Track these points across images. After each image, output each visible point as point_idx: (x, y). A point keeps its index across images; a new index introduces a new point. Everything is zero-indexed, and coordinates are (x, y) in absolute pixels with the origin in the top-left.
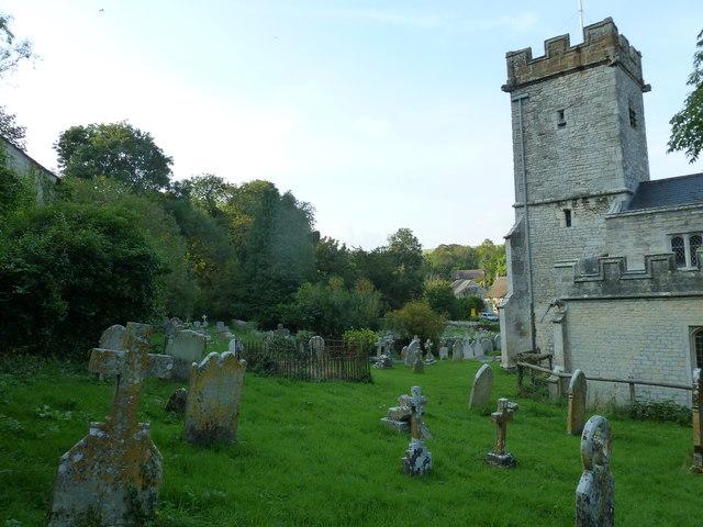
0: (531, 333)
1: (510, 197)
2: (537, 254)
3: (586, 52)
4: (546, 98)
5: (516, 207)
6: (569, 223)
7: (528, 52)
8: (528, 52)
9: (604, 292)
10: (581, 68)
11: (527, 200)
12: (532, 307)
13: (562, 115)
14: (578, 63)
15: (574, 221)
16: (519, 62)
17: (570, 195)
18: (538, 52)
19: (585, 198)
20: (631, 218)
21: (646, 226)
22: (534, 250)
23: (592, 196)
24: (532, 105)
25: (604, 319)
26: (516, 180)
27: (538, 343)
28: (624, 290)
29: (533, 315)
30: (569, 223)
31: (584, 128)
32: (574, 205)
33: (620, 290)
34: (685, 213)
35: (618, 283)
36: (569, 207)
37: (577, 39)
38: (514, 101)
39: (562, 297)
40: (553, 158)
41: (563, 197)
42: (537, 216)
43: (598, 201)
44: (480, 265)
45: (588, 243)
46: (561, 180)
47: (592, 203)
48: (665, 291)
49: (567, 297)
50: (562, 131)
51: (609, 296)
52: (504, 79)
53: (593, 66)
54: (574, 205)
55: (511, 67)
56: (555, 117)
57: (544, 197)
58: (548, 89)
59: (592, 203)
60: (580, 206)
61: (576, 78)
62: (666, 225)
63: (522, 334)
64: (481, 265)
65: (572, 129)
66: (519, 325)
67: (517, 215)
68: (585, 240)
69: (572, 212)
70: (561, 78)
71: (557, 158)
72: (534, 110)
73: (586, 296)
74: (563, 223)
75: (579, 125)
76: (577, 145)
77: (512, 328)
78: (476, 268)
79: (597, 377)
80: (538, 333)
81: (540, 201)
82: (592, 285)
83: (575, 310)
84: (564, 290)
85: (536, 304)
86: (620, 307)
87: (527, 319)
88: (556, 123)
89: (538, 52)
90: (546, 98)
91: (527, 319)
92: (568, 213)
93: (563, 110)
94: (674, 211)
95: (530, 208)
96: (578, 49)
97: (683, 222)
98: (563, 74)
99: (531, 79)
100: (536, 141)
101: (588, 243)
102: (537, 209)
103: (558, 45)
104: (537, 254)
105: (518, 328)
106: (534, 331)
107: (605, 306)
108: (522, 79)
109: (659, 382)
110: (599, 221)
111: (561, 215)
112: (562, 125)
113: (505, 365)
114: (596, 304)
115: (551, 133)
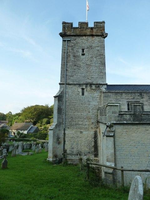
0: (63, 142)
1: (58, 79)
2: (69, 106)
3: (95, 30)
4: (77, 43)
5: (60, 84)
6: (83, 94)
7: (72, 24)
8: (72, 24)
9: (134, 120)
10: (92, 36)
11: (66, 82)
12: (64, 130)
13: (83, 51)
14: (91, 33)
15: (86, 93)
16: (67, 26)
17: (85, 82)
18: (76, 25)
19: (91, 85)
20: (114, 94)
21: (119, 97)
22: (67, 104)
23: (94, 84)
24: (71, 44)
25: (134, 134)
26: (61, 73)
27: (66, 148)
28: (144, 120)
29: (64, 134)
30: (83, 94)
31: (92, 57)
32: (86, 87)
33: (142, 120)
34: (133, 94)
35: (141, 116)
36: (84, 87)
37: (91, 25)
38: (64, 41)
39: (112, 122)
40: (79, 67)
41: (82, 83)
42: (70, 89)
43: (96, 87)
44: (7, 119)
45: (91, 103)
46: (80, 76)
47: (94, 87)
48: (137, 121)
49: (115, 122)
50: (83, 57)
51: (137, 122)
52: (61, 31)
53: (97, 36)
54: (86, 87)
55: (64, 28)
56: (81, 51)
57: (73, 82)
58: (79, 40)
59: (94, 87)
60: (89, 88)
61: (90, 39)
62: (127, 98)
63: (59, 143)
64: (7, 119)
65: (87, 57)
66: (58, 138)
67: (61, 88)
68: (90, 102)
69: (85, 90)
70: (84, 37)
71: (80, 67)
72: (72, 46)
73: (125, 122)
74: (81, 94)
75: (90, 56)
76: (89, 63)
77: (55, 140)
78: (5, 120)
79: (131, 169)
80: (66, 143)
81: (72, 83)
82: (128, 116)
83: (118, 129)
84: (113, 118)
85: (66, 129)
86: (142, 128)
87: (61, 136)
88: (81, 53)
89: (76, 25)
90: (77, 43)
91: (61, 136)
92: (83, 89)
93: (84, 49)
94: (130, 93)
95: (67, 86)
96: (92, 28)
97: (132, 97)
98: (85, 36)
99: (72, 34)
100: (72, 58)
101: (91, 103)
102: (70, 86)
103: (83, 25)
104: (69, 106)
105: (57, 140)
106: (65, 141)
107: (135, 127)
108: (68, 33)
109: (144, 169)
110: (96, 94)
111: (80, 90)
112: (83, 55)
113: (51, 159)
114: (130, 127)
115: (78, 56)
